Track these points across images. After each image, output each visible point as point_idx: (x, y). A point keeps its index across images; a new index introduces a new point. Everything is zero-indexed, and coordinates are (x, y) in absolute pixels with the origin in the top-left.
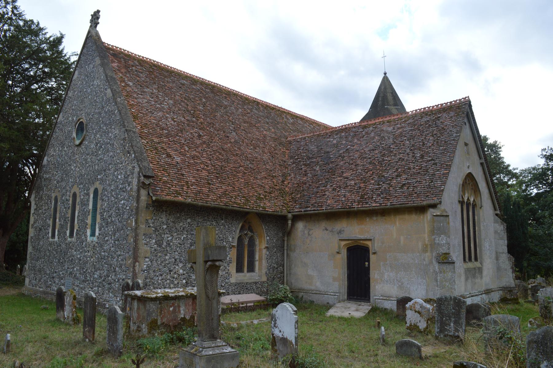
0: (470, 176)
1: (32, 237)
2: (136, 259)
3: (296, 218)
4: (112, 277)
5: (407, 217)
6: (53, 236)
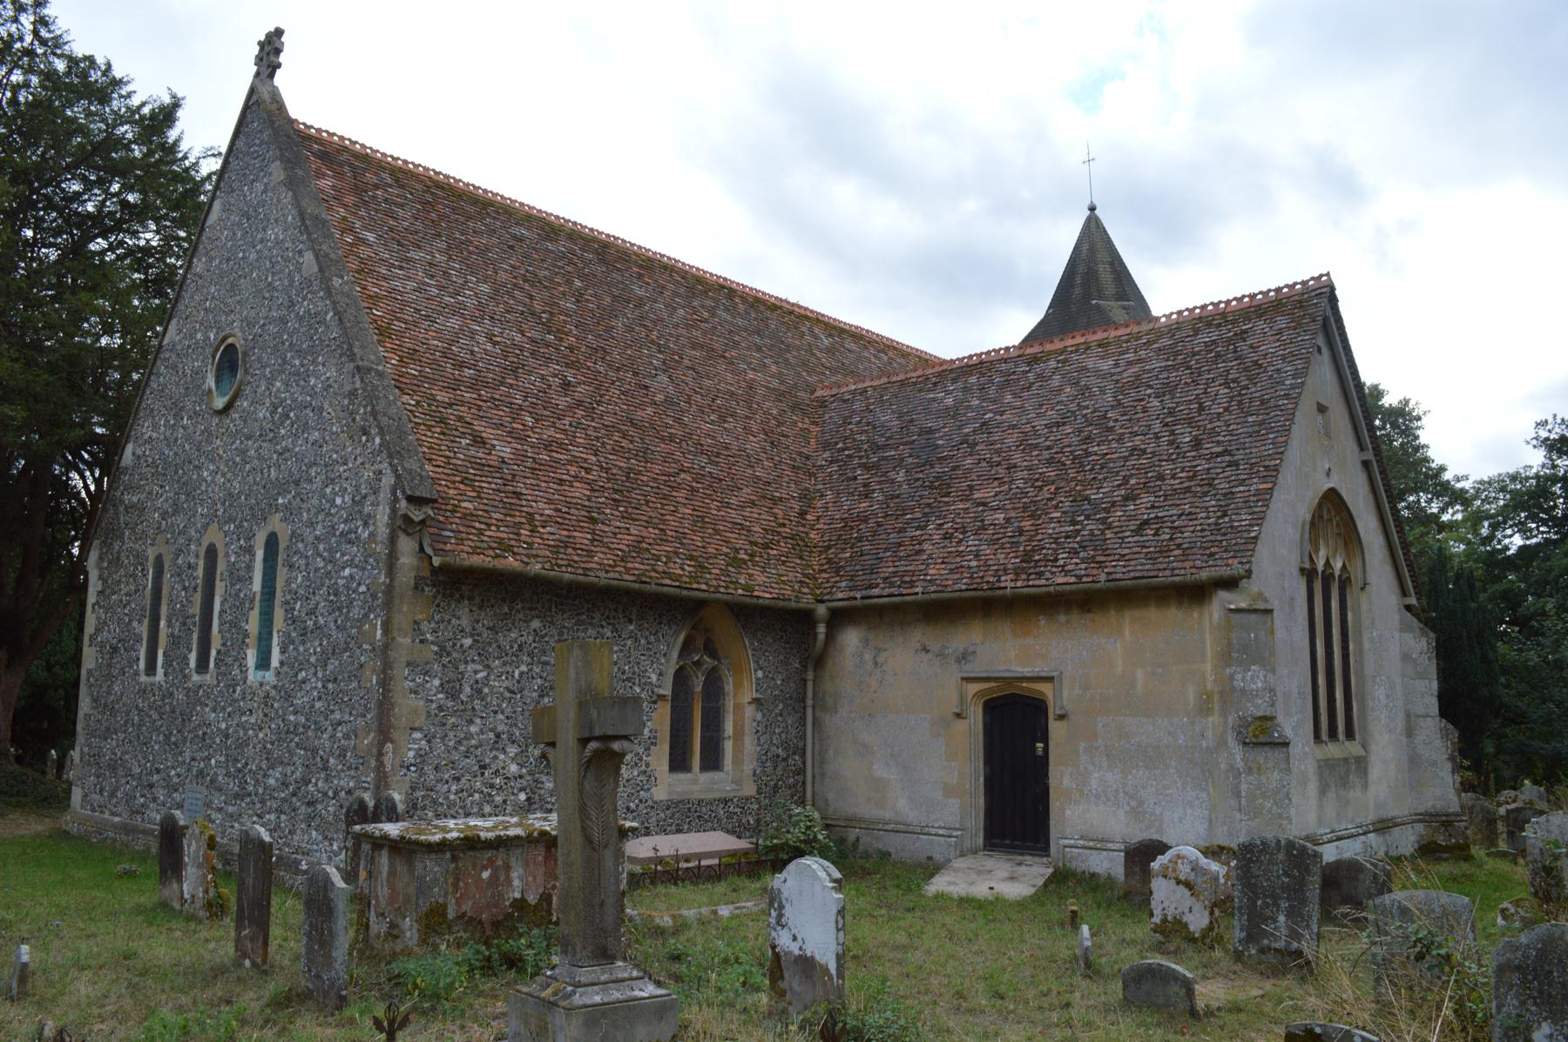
0: (1332, 499)
1: (89, 672)
2: (384, 733)
3: (841, 617)
4: (319, 783)
5: (1153, 613)
6: (151, 668)
